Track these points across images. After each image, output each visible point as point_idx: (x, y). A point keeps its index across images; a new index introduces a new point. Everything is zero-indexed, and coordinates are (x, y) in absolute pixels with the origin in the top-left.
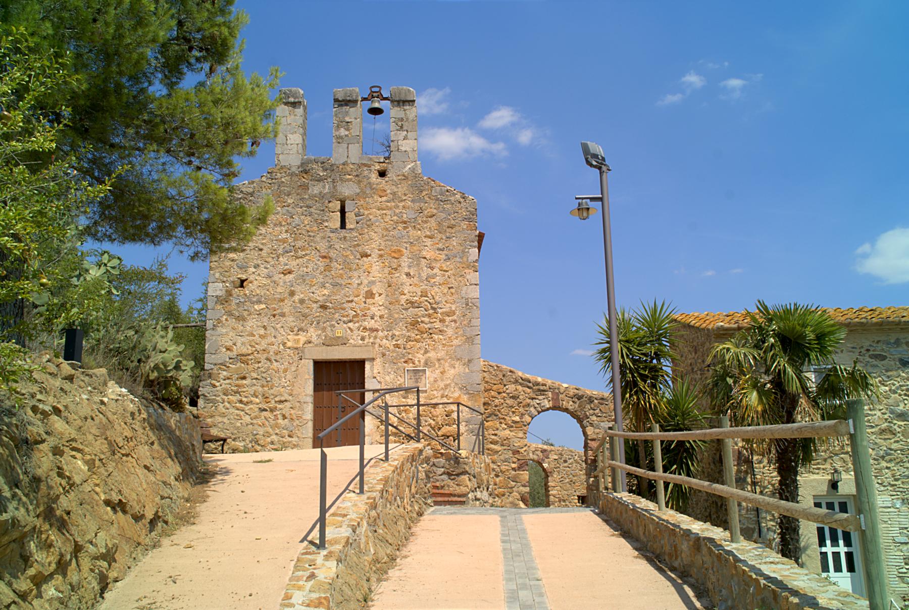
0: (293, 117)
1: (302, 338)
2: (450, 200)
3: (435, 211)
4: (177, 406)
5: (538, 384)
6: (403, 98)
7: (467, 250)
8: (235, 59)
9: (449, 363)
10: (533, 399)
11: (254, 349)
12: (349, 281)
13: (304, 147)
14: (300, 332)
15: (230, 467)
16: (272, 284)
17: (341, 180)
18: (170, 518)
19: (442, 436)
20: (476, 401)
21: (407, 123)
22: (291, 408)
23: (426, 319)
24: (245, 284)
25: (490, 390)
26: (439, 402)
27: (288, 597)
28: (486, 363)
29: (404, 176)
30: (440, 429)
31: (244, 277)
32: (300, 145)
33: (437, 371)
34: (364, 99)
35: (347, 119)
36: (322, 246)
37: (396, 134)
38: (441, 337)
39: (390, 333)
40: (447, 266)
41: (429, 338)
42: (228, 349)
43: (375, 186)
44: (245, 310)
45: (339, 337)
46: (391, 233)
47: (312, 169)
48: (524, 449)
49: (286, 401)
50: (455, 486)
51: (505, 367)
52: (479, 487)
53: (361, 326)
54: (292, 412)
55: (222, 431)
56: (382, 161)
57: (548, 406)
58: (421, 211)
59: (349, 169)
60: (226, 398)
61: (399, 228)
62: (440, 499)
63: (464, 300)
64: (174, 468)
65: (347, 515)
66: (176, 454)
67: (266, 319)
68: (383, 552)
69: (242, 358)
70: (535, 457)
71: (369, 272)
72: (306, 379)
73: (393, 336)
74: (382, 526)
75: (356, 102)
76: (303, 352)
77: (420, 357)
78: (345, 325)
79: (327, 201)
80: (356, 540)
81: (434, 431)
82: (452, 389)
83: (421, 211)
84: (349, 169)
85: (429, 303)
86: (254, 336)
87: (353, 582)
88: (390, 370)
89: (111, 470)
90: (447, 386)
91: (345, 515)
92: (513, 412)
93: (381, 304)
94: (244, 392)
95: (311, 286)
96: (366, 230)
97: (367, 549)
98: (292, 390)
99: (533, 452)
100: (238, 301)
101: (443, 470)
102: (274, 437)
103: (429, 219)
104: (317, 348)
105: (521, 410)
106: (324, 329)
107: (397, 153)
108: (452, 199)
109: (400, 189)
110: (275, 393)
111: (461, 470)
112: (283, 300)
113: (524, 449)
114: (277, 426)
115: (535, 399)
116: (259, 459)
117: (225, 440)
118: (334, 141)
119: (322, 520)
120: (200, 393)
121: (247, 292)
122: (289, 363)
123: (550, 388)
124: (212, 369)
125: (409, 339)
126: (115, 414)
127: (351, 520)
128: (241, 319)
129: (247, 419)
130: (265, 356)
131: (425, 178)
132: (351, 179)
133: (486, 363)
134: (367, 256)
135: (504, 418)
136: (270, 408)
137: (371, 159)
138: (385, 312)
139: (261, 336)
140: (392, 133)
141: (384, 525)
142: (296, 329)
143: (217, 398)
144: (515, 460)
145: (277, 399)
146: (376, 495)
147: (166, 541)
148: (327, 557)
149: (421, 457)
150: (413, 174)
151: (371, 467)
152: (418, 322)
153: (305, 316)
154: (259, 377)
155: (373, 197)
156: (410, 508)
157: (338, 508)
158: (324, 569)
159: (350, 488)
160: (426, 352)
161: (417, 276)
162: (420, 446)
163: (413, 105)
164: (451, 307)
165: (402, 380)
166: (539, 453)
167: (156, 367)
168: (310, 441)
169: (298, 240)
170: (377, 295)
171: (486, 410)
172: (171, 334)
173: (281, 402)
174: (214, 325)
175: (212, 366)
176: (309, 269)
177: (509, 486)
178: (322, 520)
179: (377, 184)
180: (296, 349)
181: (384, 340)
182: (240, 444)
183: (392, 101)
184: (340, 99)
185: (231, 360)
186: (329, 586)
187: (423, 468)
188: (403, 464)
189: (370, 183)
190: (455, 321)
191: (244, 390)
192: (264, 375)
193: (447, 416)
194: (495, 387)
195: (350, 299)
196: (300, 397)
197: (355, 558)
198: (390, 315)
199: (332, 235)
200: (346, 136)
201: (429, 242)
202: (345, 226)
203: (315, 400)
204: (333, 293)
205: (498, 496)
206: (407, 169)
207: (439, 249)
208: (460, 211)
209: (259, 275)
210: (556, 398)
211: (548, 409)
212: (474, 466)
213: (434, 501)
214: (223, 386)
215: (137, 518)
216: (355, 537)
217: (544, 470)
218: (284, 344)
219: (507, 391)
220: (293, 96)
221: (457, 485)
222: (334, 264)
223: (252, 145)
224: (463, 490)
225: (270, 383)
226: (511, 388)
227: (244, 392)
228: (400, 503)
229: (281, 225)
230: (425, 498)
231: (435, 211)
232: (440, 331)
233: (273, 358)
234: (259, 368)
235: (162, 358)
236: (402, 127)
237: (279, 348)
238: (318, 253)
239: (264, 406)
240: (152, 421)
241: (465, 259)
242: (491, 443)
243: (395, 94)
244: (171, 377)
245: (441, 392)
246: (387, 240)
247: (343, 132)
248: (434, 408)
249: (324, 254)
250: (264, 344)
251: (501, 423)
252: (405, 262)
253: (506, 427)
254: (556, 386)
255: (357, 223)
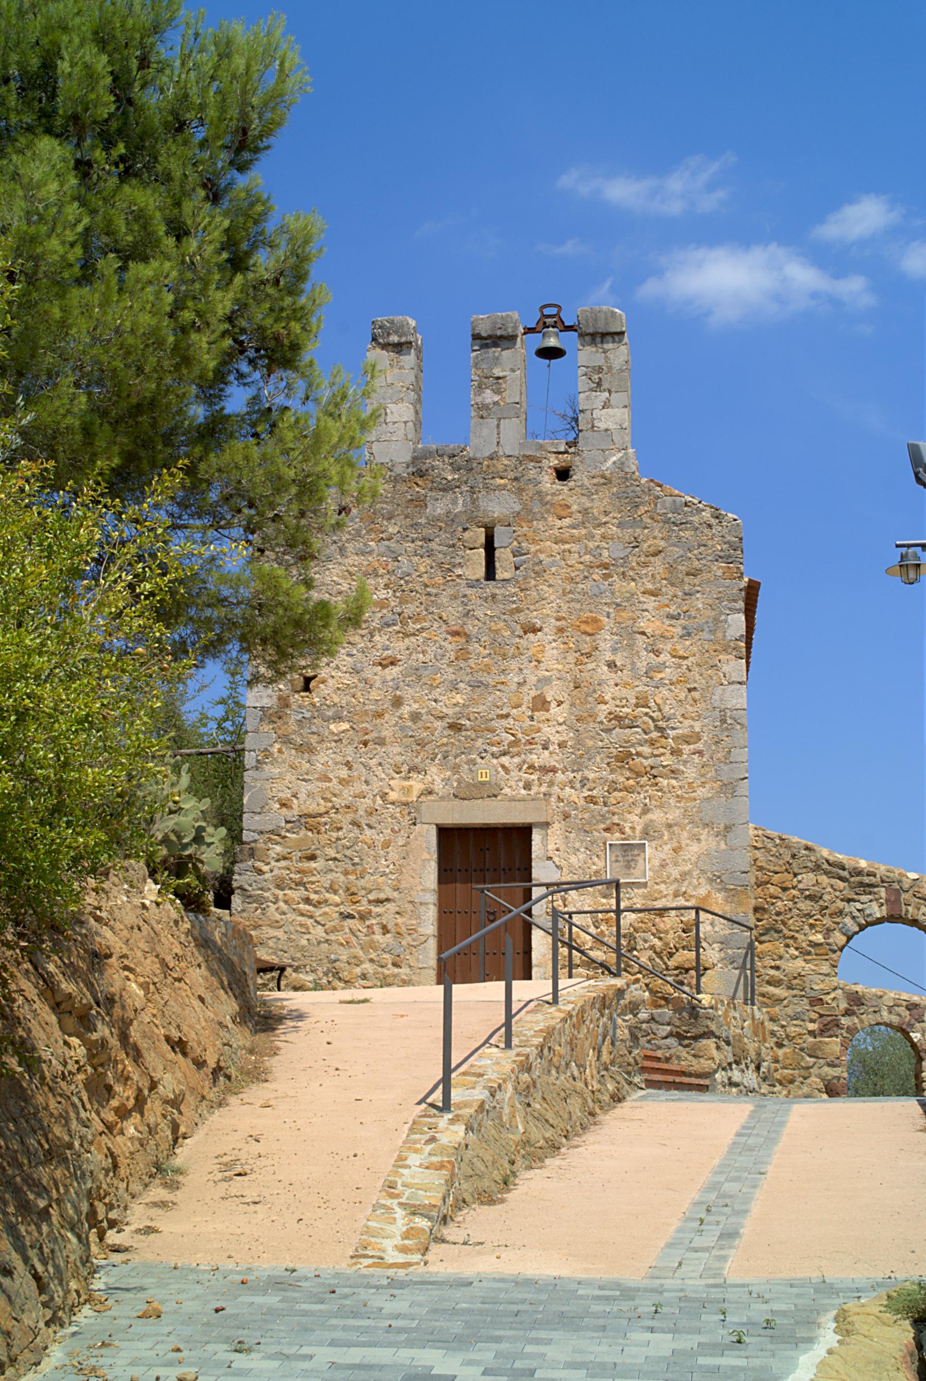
0: (396, 371)
1: (417, 784)
2: (691, 523)
3: (662, 544)
4: (198, 907)
5: (859, 873)
6: (601, 328)
7: (723, 617)
8: (311, 352)
9: (690, 832)
10: (849, 901)
11: (330, 805)
12: (502, 678)
13: (418, 424)
14: (414, 775)
15: (304, 1009)
16: (361, 685)
17: (486, 487)
18: (233, 1071)
19: (676, 968)
20: (740, 904)
21: (608, 377)
22: (398, 913)
23: (646, 750)
24: (312, 684)
25: (768, 883)
26: (670, 905)
27: (401, 1158)
28: (760, 832)
29: (603, 477)
30: (671, 955)
31: (310, 673)
32: (410, 424)
33: (667, 848)
34: (529, 331)
35: (497, 372)
36: (452, 612)
37: (588, 398)
38: (673, 782)
39: (579, 776)
40: (686, 649)
41: (652, 786)
42: (283, 805)
43: (549, 498)
44: (313, 733)
45: (483, 784)
46: (580, 586)
47: (433, 468)
48: (832, 995)
49: (388, 900)
50: (690, 1058)
51: (795, 839)
52: (737, 1063)
53: (524, 762)
54: (400, 920)
55: (275, 954)
56: (562, 449)
57: (878, 915)
58: (636, 543)
59: (500, 467)
60: (280, 893)
61: (595, 577)
62: (657, 1077)
63: (717, 712)
64: (228, 1006)
65: (483, 1075)
66: (229, 984)
67: (350, 750)
68: (538, 1134)
69: (308, 821)
70: (895, 1019)
71: (539, 662)
72: (424, 861)
73: (584, 781)
74: (539, 1098)
75: (512, 338)
76: (418, 810)
77: (633, 821)
78: (495, 761)
79: (460, 529)
80: (495, 1107)
81: (661, 958)
82: (695, 881)
83: (636, 543)
84: (500, 467)
85: (651, 718)
86: (330, 780)
87: (488, 1158)
88: (577, 845)
89: (166, 997)
90: (684, 875)
91: (481, 1075)
92: (812, 926)
93: (561, 720)
94: (313, 883)
95: (432, 687)
96: (533, 582)
97: (514, 1124)
98: (399, 881)
99: (890, 1009)
100: (301, 716)
101: (669, 1028)
102: (367, 967)
103: (652, 559)
104: (444, 804)
105: (827, 921)
106: (456, 768)
107: (590, 433)
108: (695, 519)
109: (597, 503)
110: (368, 886)
111: (701, 1030)
112: (380, 715)
113: (832, 995)
114: (372, 946)
115: (854, 900)
116: (349, 998)
117: (282, 969)
118: (473, 414)
119: (446, 1082)
120: (235, 884)
121: (317, 700)
122: (393, 830)
123: (883, 881)
124: (255, 841)
125: (613, 787)
126: (159, 922)
127: (490, 1080)
128: (305, 749)
129: (319, 932)
130: (350, 817)
131: (644, 481)
132: (505, 486)
133: (760, 832)
134: (535, 630)
135: (792, 937)
136: (359, 912)
137: (541, 447)
138: (568, 736)
139: (342, 781)
140: (582, 396)
141: (544, 1099)
142: (405, 768)
143: (265, 894)
144: (814, 1016)
145: (372, 897)
146: (533, 1052)
147: (233, 1100)
148: (452, 1121)
149: (622, 1002)
150: (622, 474)
151: (528, 1012)
152: (631, 754)
153: (422, 744)
154: (339, 856)
155: (545, 519)
156: (596, 1086)
157: (472, 1066)
158: (448, 1133)
159: (492, 1041)
160: (646, 810)
161: (629, 667)
162: (619, 982)
163: (620, 341)
164: (692, 727)
165: (601, 864)
166: (902, 1010)
167: (165, 841)
168: (433, 974)
169: (407, 602)
170: (554, 704)
171: (759, 920)
172: (185, 780)
173: (379, 902)
174: (258, 761)
175: (257, 837)
176: (427, 658)
177: (803, 1064)
178: (446, 1082)
179: (554, 494)
180: (406, 804)
181: (567, 789)
182: (307, 978)
183: (582, 335)
184: (484, 334)
185: (290, 825)
186: (454, 1151)
187: (624, 1021)
188: (582, 1010)
189: (539, 493)
190: (700, 753)
191: (313, 879)
192: (348, 853)
193: (684, 931)
194: (776, 878)
195: (504, 712)
196: (413, 893)
197: (493, 1131)
198: (579, 742)
199: (469, 592)
200: (496, 403)
201: (650, 603)
202: (494, 574)
203: (440, 899)
204: (473, 701)
205: (781, 1084)
206: (609, 463)
207: (670, 617)
208: (710, 543)
209: (337, 668)
210: (894, 899)
211: (879, 921)
212: (728, 1024)
213: (646, 1080)
214: (276, 872)
215: (200, 1064)
216: (494, 1104)
217: (913, 1045)
218: (384, 796)
219: (800, 886)
220: (396, 332)
221: (694, 1056)
222: (475, 647)
223: (340, 513)
224: (705, 1065)
225: (359, 868)
226: (808, 879)
227: (313, 883)
228: (576, 1073)
229: (377, 576)
230: (629, 1073)
231: (662, 544)
232: (673, 772)
233: (363, 822)
234: (338, 839)
235: (176, 824)
236: (599, 384)
237: (374, 802)
238: (444, 627)
239: (349, 910)
240: (196, 933)
241: (720, 635)
242: (769, 983)
243: (587, 321)
244: (190, 856)
245: (674, 886)
246: (573, 600)
247: (489, 397)
248: (661, 916)
249: (455, 628)
250: (347, 796)
251: (787, 946)
252: (606, 641)
253: (796, 953)
254: (895, 875)
255: (517, 568)
